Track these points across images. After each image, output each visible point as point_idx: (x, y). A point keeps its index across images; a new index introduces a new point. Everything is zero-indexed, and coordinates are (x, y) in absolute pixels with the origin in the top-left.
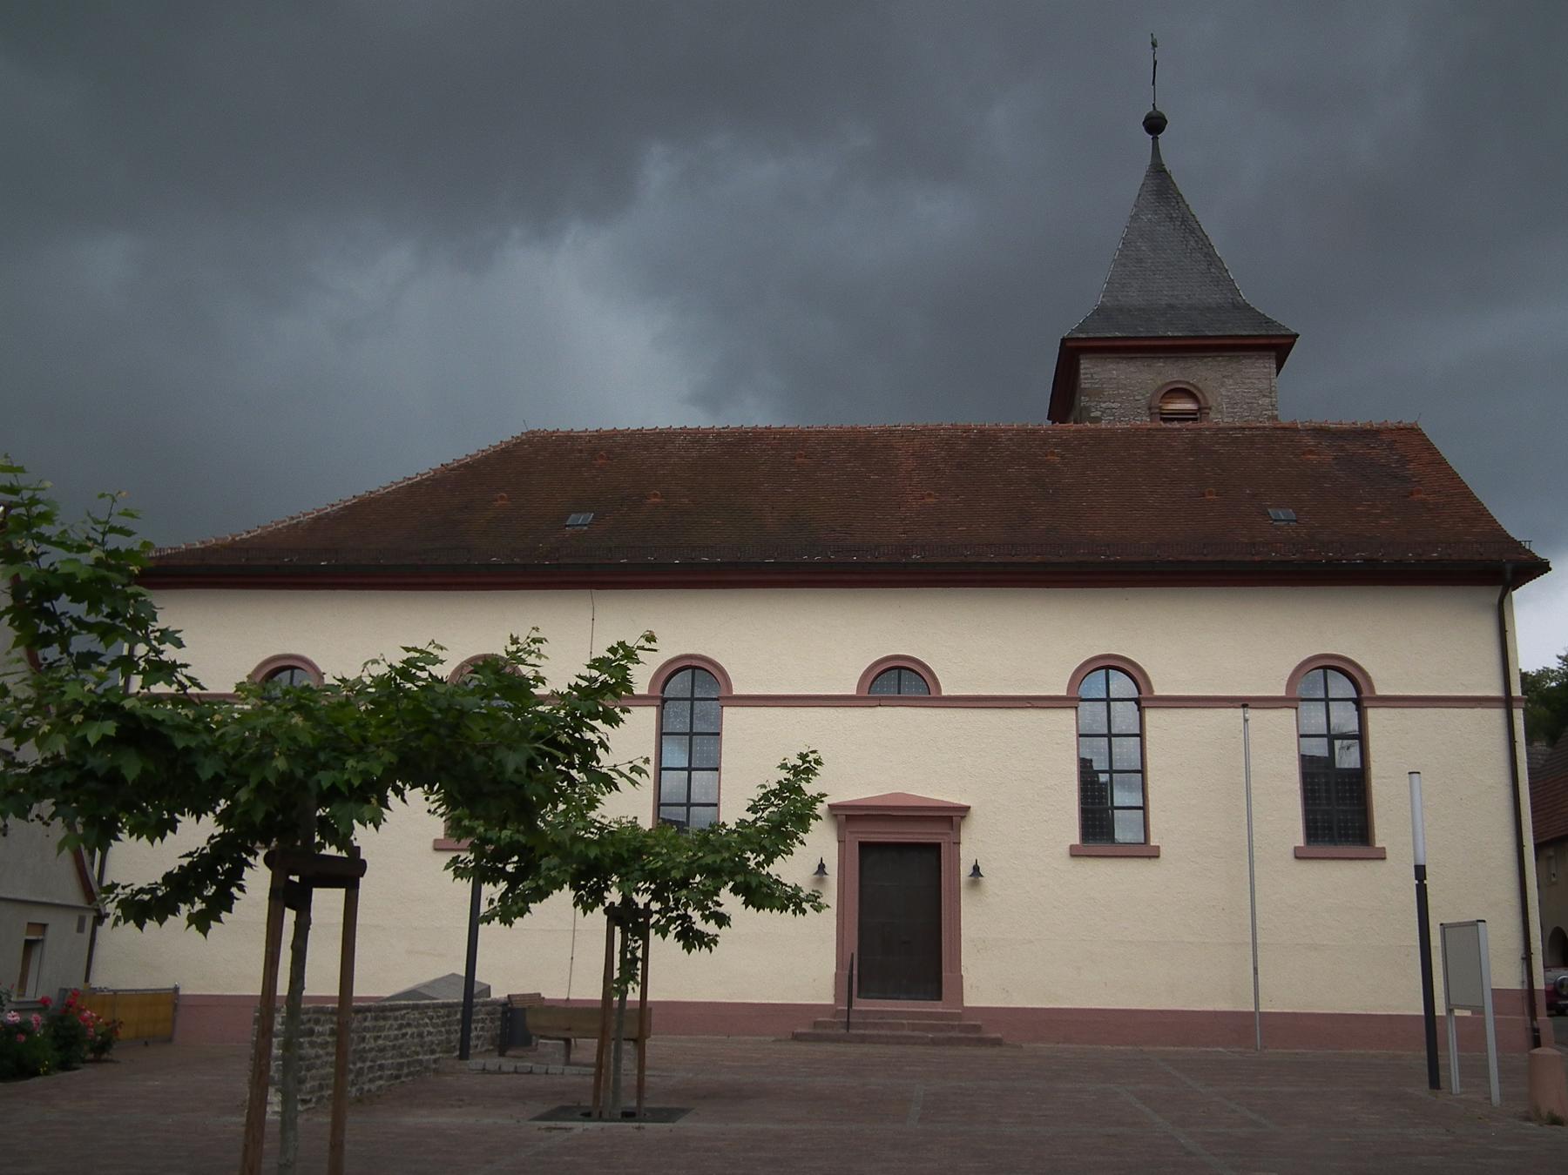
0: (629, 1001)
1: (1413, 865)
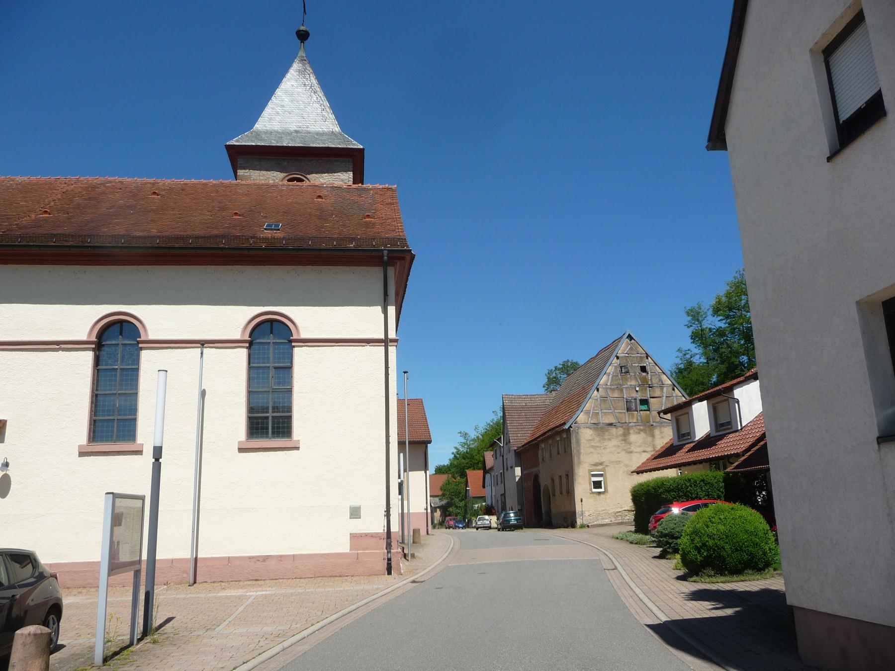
1: (237, 448)
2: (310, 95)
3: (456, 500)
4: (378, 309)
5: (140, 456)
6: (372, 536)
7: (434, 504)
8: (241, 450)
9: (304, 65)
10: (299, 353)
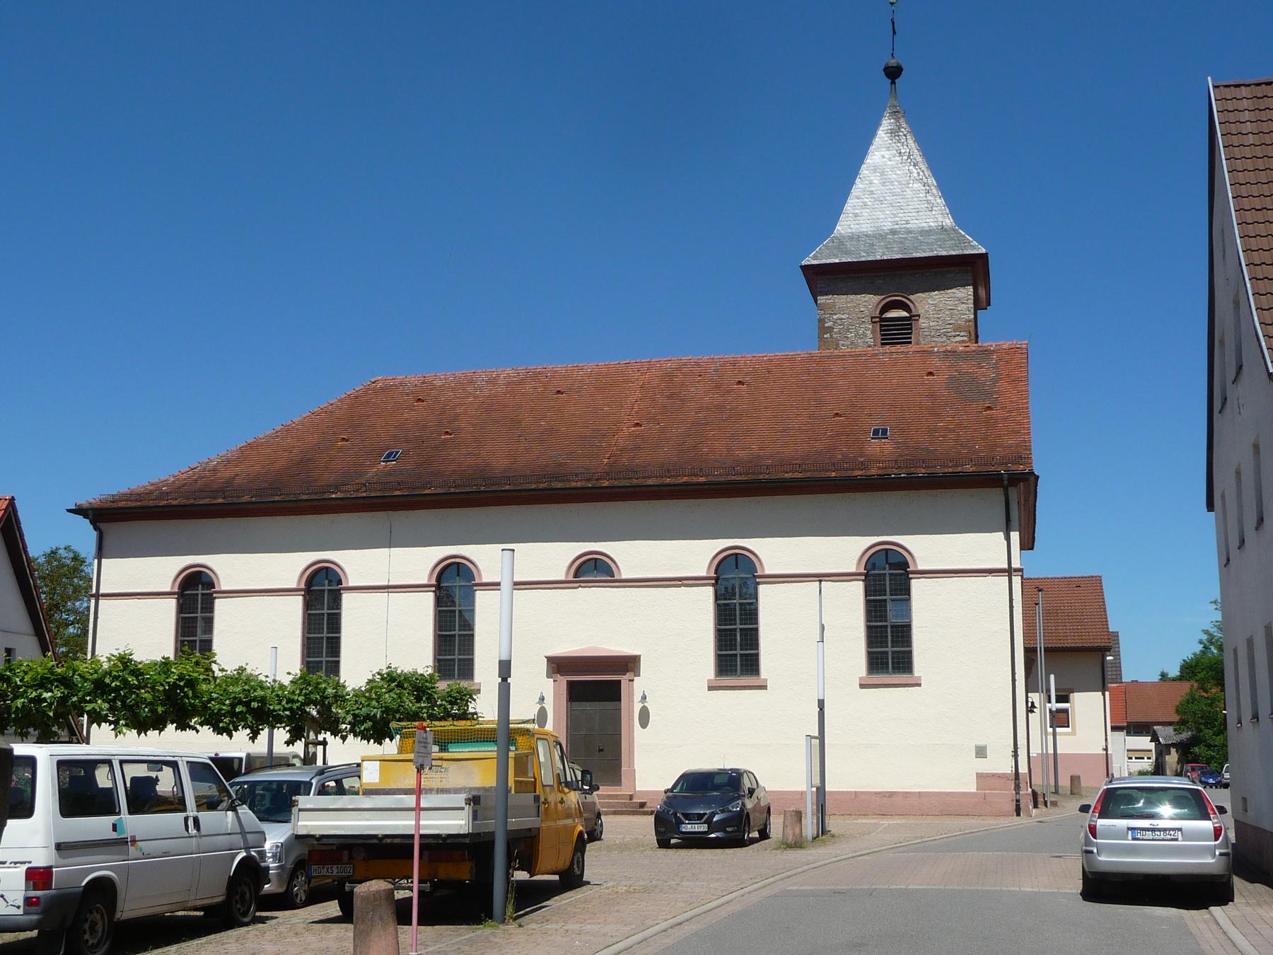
2: (909, 170)
3: (1208, 733)
4: (1001, 535)
5: (765, 691)
6: (988, 776)
7: (1164, 739)
9: (897, 120)
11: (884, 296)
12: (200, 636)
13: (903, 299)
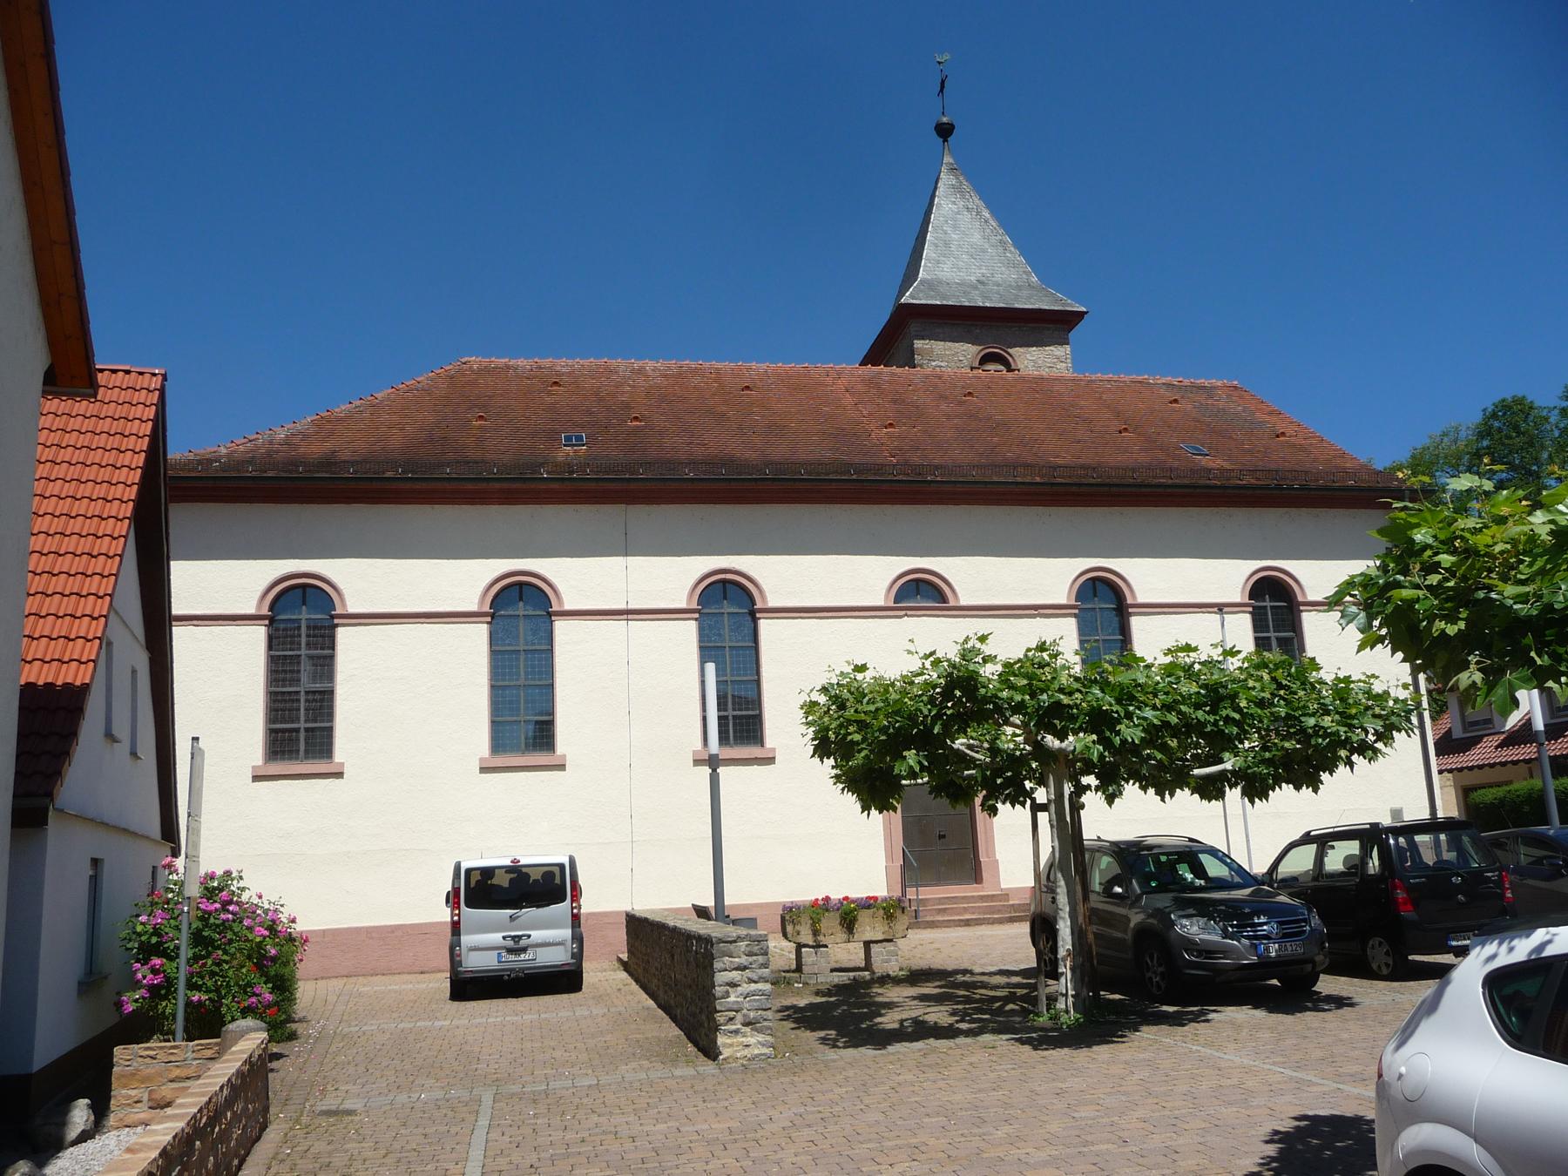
0: (727, 906)
8: (484, 770)
10: (561, 627)
11: (982, 347)
12: (306, 683)
13: (1001, 352)
